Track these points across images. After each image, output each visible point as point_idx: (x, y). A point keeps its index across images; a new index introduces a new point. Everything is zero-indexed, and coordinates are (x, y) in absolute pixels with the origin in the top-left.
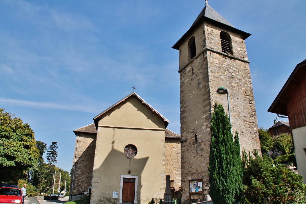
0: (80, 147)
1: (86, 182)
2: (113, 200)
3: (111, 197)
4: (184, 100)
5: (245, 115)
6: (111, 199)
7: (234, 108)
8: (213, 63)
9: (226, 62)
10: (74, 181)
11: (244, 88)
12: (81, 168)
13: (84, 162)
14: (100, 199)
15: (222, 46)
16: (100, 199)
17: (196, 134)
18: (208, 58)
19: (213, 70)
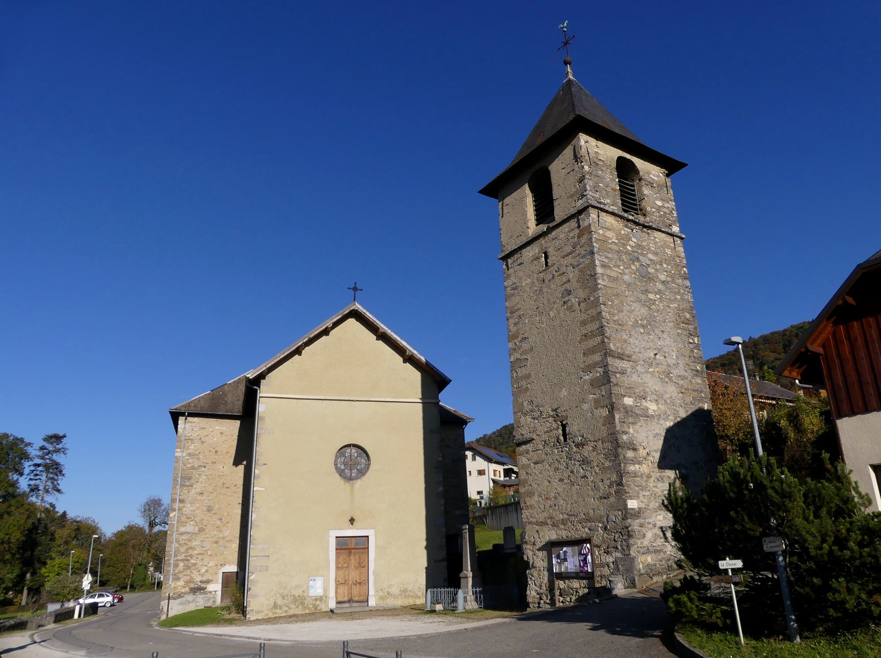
0: (190, 455)
1: (211, 555)
2: (311, 602)
3: (305, 594)
4: (521, 332)
5: (682, 373)
6: (305, 599)
7: (658, 357)
8: (604, 241)
9: (633, 239)
10: (176, 556)
11: (676, 306)
13: (204, 498)
15: (622, 195)
16: (275, 602)
17: (564, 422)
18: (593, 229)
19: (606, 261)
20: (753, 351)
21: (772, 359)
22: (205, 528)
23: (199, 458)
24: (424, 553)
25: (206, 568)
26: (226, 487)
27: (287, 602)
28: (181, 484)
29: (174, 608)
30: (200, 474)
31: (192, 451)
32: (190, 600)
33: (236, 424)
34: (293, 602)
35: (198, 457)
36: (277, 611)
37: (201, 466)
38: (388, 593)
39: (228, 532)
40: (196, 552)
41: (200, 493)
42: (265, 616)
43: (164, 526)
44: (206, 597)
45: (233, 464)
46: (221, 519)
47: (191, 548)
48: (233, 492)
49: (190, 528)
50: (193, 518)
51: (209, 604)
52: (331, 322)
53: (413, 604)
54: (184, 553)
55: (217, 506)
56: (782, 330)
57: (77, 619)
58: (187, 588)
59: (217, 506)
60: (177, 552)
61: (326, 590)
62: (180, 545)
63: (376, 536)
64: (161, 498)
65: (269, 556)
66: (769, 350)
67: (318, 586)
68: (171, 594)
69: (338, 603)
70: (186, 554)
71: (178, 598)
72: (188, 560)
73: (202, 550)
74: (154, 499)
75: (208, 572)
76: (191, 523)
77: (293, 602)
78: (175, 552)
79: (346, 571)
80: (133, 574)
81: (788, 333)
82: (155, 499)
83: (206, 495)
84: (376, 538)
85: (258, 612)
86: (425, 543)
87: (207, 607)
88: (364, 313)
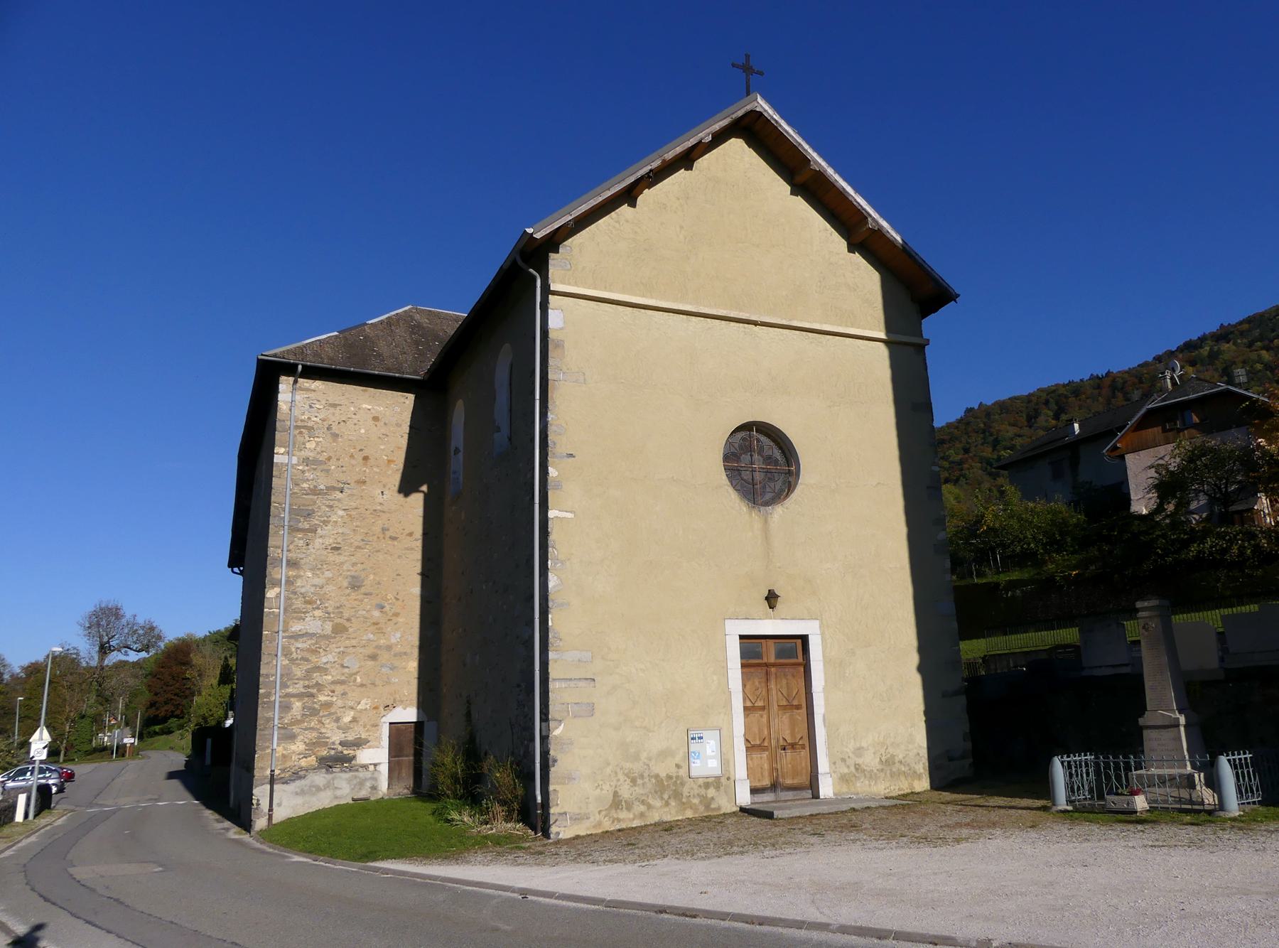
0: (306, 461)
1: (362, 685)
2: (696, 792)
3: (683, 772)
6: (683, 784)
10: (284, 686)
12: (323, 599)
13: (342, 558)
14: (616, 794)
16: (616, 794)
20: (985, 424)
21: (1010, 434)
22: (347, 624)
23: (328, 471)
24: (917, 680)
25: (352, 713)
26: (390, 538)
27: (642, 792)
28: (290, 526)
29: (283, 804)
30: (331, 507)
31: (311, 454)
32: (321, 785)
33: (407, 402)
34: (656, 792)
35: (325, 467)
36: (623, 815)
37: (334, 488)
38: (857, 767)
39: (398, 635)
40: (329, 677)
41: (332, 549)
42: (594, 827)
43: (126, 652)
44: (356, 777)
45: (400, 491)
46: (383, 607)
47: (318, 669)
48: (407, 549)
49: (313, 624)
50: (318, 602)
51: (363, 793)
52: (708, 131)
53: (909, 791)
54: (301, 679)
55: (372, 577)
56: (1027, 394)
57: (22, 824)
58: (313, 757)
59: (372, 577)
60: (287, 676)
61: (726, 761)
62: (292, 661)
63: (823, 634)
64: (120, 605)
65: (594, 680)
66: (1006, 423)
67: (709, 752)
68: (277, 772)
69: (754, 791)
70: (307, 683)
71: (293, 781)
72: (312, 696)
73: (343, 674)
74: (107, 607)
75: (357, 722)
76: (318, 613)
77: (656, 792)
78: (282, 675)
79: (762, 716)
80: (69, 732)
81: (1034, 399)
82: (110, 607)
83: (347, 554)
84: (823, 640)
85: (577, 819)
86: (914, 659)
87: (361, 799)
88: (776, 122)
